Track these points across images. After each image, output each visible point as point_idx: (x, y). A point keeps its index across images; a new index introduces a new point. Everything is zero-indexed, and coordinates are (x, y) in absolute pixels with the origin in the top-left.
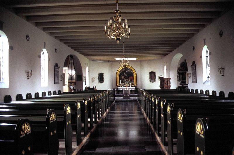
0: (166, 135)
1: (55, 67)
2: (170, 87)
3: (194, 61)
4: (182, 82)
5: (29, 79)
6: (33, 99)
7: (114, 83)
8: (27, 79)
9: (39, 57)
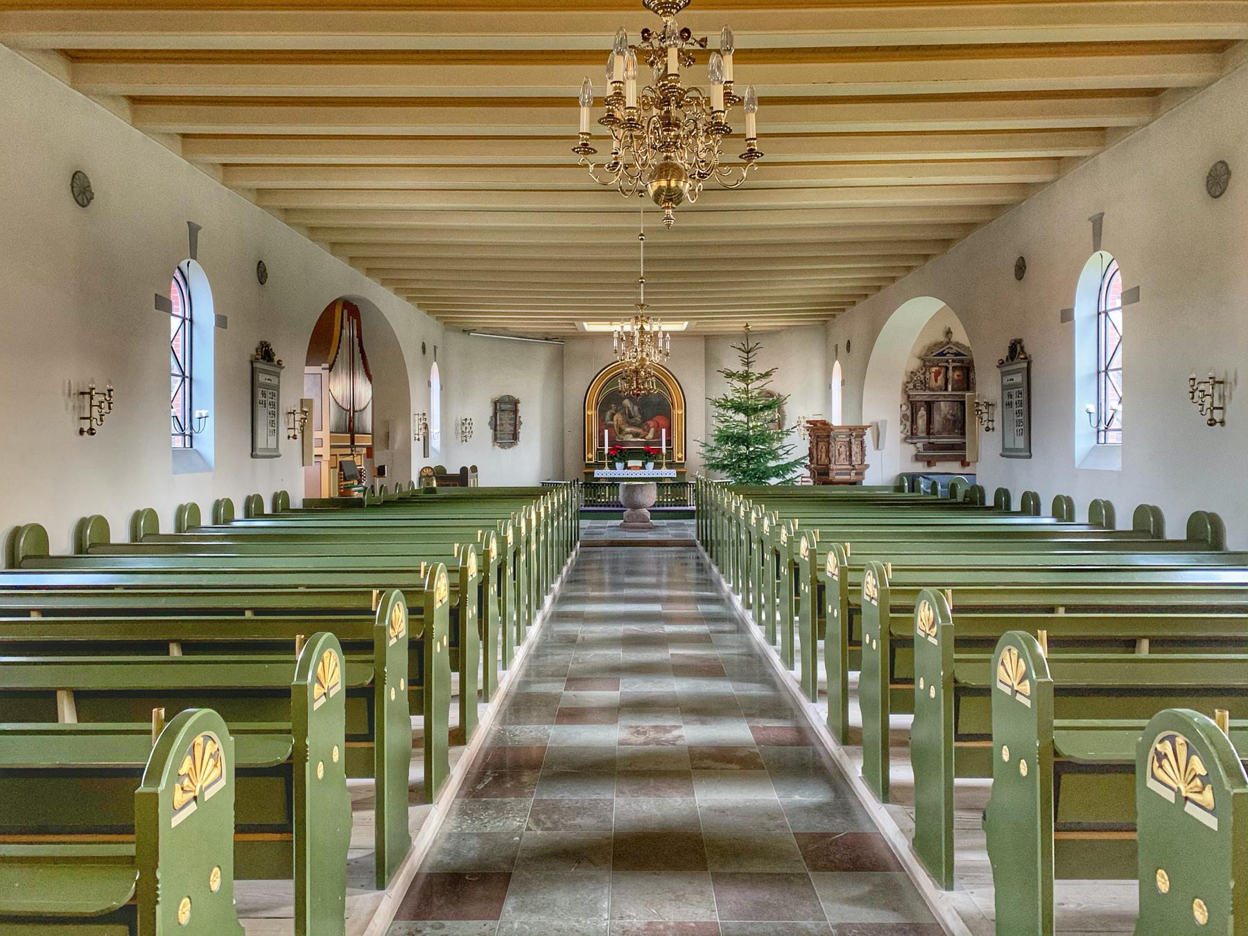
0: (761, 607)
1: (257, 365)
2: (860, 474)
3: (1020, 341)
4: (930, 446)
5: (91, 432)
6: (121, 549)
7: (572, 443)
8: (82, 432)
9: (225, 318)
